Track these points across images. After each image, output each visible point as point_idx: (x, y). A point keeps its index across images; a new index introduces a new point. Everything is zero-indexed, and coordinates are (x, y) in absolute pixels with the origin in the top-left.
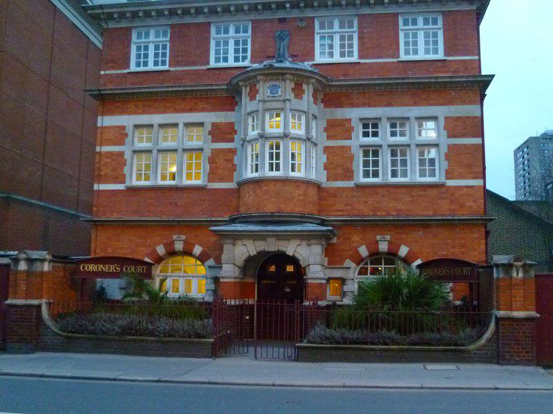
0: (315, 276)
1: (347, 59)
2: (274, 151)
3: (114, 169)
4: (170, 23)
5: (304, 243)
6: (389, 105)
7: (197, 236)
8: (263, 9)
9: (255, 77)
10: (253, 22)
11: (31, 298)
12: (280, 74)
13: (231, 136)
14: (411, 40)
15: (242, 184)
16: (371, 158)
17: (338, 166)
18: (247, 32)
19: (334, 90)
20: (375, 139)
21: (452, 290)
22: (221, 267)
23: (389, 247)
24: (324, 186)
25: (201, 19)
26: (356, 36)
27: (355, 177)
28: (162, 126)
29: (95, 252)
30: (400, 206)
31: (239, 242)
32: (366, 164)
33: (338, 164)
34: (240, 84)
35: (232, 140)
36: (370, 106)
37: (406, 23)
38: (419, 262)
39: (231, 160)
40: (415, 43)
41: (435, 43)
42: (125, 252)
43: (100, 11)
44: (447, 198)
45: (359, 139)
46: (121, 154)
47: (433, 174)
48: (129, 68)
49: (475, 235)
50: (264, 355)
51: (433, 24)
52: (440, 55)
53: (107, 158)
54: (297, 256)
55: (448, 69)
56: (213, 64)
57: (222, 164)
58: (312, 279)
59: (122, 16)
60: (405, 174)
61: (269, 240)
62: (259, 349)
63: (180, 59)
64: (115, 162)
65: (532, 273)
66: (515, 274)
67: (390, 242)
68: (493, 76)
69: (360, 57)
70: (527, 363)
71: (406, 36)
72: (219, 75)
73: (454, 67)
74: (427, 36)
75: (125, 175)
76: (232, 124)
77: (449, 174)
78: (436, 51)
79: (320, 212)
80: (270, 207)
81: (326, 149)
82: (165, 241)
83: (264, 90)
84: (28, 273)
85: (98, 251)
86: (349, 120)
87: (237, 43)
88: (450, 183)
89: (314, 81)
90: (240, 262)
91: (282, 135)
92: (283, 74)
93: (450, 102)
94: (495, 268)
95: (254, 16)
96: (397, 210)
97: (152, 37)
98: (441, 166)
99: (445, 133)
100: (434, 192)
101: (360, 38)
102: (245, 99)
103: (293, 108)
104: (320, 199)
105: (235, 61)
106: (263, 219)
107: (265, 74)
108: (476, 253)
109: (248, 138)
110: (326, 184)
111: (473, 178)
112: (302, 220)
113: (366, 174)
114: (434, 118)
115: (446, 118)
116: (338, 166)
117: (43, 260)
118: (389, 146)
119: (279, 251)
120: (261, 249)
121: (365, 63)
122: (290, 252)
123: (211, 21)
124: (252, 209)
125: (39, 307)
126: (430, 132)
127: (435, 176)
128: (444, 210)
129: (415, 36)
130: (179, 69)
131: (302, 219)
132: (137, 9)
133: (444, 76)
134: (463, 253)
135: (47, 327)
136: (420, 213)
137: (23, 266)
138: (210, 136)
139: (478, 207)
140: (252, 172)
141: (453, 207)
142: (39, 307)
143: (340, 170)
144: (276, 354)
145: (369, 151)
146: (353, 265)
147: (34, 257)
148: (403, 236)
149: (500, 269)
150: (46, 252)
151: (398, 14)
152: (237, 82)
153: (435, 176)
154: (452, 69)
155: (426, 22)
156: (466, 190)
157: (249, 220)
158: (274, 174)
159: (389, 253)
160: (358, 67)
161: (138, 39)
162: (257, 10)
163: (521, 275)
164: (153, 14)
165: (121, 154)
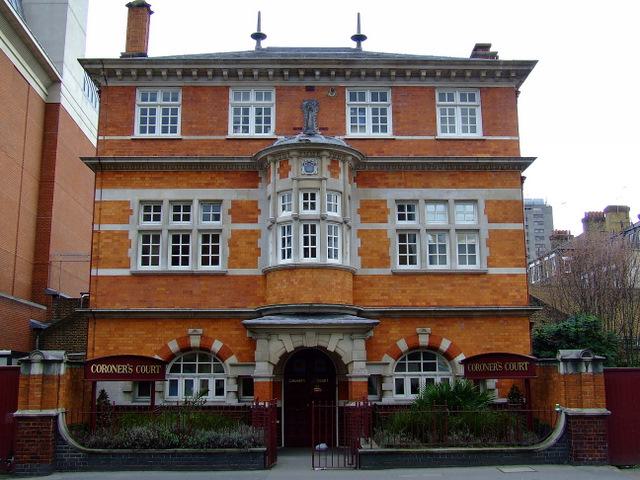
0: (360, 374)
1: (380, 135)
2: (310, 235)
3: (116, 251)
4: (182, 84)
5: (347, 337)
6: (427, 186)
7: (216, 329)
8: (305, 75)
9: (288, 152)
10: (278, 89)
11: (47, 408)
12: (316, 151)
13: (255, 216)
14: (241, 116)
15: (267, 272)
16: (210, 244)
17: (372, 251)
18: (270, 99)
19: (369, 168)
20: (411, 223)
21: (497, 386)
22: (254, 365)
23: (450, 346)
24: (358, 273)
25: (218, 82)
26: (389, 111)
27: (392, 264)
28: (457, 201)
29: (93, 349)
30: (441, 296)
31: (274, 337)
32: (145, 250)
33: (372, 251)
34: (269, 159)
35: (255, 221)
36: (406, 187)
37: (237, 97)
38: (461, 357)
39: (254, 243)
40: (452, 120)
41: (473, 121)
42: (130, 348)
43: (100, 66)
44: (488, 287)
45: (394, 224)
46: (125, 234)
47: (473, 261)
48: (133, 134)
49: (520, 327)
50: (323, 462)
51: (470, 101)
52: (479, 135)
53: (107, 238)
54: (339, 352)
55: (487, 149)
56: (137, 134)
57: (248, 247)
58: (356, 377)
59: (217, 73)
60: (443, 261)
61: (308, 334)
62: (316, 458)
63: (194, 126)
64: (116, 243)
65: (601, 368)
66: (584, 369)
67: (202, 336)
68: (534, 159)
69: (395, 133)
70: (601, 462)
71: (443, 112)
72: (240, 146)
73: (494, 147)
74: (464, 112)
75: (129, 259)
76: (256, 202)
77: (491, 262)
78: (474, 130)
79: (355, 301)
80: (306, 298)
81: (360, 233)
82: (179, 336)
83: (297, 167)
84: (45, 378)
85: (97, 348)
86: (385, 201)
87: (165, 112)
88: (493, 271)
89: (350, 158)
90: (275, 360)
91: (319, 218)
92: (319, 151)
93: (490, 185)
94: (561, 364)
95: (279, 82)
96: (437, 300)
97: (253, 99)
98: (482, 253)
99: (485, 218)
100: (475, 281)
101: (395, 113)
102: (274, 175)
103: (329, 187)
104: (354, 289)
105: (141, 132)
106: (300, 311)
107: (300, 151)
108: (521, 346)
109: (278, 220)
110: (360, 272)
111: (516, 266)
112: (342, 311)
113: (403, 261)
114: (474, 202)
115: (487, 202)
116: (372, 251)
117: (60, 362)
118: (200, 231)
119: (302, 347)
120: (300, 344)
121: (401, 140)
122: (331, 348)
123: (229, 84)
124: (285, 300)
125: (56, 417)
126: (466, 217)
127: (475, 263)
128: (486, 300)
129: (452, 112)
130: (192, 137)
131: (340, 311)
132: (144, 67)
133: (484, 156)
134: (508, 346)
135: (65, 442)
136: (462, 303)
137: (37, 370)
138: (230, 216)
139: (522, 297)
140: (284, 258)
141: (495, 297)
142: (56, 417)
143: (375, 257)
144: (342, 463)
145: (149, 236)
146: (391, 361)
147: (50, 358)
148: (445, 328)
149: (569, 364)
150: (63, 352)
151: (435, 88)
152: (265, 158)
153: (475, 263)
154: (492, 150)
155: (463, 98)
156: (508, 278)
157: (282, 311)
158: (310, 260)
159: (429, 347)
160: (393, 143)
161: (235, 99)
162: (404, 76)
163: (590, 370)
164: (164, 73)
165: (125, 234)
